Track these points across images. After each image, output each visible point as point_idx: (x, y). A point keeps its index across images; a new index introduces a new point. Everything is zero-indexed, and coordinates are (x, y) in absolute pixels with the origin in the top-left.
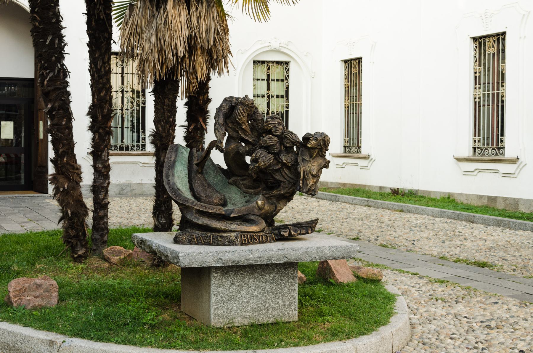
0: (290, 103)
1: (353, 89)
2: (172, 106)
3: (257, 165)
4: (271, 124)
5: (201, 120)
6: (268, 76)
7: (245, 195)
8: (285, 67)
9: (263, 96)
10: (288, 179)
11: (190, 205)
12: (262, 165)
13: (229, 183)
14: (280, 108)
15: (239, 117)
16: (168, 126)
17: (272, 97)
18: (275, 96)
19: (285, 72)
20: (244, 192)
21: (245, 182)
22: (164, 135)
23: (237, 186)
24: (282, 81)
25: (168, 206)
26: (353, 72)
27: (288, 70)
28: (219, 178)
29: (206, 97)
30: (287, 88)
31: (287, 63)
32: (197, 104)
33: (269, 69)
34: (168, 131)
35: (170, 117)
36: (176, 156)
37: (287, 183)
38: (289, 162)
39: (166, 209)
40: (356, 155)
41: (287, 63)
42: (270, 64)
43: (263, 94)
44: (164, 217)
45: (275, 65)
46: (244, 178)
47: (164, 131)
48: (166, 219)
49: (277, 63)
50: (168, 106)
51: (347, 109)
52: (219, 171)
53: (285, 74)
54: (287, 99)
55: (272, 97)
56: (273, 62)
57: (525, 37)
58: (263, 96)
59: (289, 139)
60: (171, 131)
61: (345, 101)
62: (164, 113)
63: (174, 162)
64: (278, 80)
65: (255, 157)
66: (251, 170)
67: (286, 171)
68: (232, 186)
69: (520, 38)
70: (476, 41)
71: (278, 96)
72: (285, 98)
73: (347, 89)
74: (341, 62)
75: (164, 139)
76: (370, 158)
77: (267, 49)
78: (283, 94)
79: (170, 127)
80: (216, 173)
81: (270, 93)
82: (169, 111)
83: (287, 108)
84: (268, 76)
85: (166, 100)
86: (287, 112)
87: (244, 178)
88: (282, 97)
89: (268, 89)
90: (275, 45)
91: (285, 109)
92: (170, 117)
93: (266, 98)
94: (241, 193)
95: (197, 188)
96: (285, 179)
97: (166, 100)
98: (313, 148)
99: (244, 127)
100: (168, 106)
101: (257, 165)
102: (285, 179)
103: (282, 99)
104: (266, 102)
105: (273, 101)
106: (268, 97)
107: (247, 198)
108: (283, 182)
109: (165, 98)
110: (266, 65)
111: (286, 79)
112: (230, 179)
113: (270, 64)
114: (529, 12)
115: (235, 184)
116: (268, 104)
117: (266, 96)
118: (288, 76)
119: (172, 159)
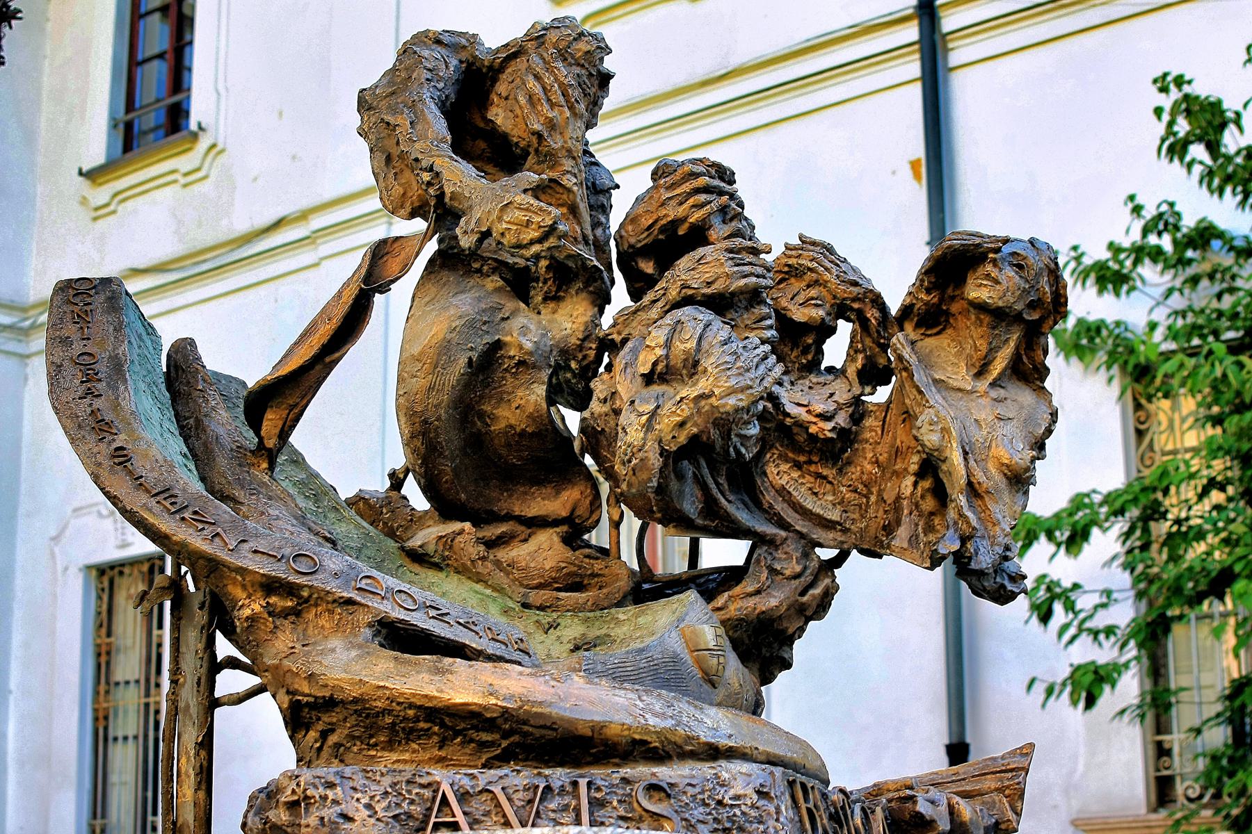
12: (732, 391)
73: (103, 659)
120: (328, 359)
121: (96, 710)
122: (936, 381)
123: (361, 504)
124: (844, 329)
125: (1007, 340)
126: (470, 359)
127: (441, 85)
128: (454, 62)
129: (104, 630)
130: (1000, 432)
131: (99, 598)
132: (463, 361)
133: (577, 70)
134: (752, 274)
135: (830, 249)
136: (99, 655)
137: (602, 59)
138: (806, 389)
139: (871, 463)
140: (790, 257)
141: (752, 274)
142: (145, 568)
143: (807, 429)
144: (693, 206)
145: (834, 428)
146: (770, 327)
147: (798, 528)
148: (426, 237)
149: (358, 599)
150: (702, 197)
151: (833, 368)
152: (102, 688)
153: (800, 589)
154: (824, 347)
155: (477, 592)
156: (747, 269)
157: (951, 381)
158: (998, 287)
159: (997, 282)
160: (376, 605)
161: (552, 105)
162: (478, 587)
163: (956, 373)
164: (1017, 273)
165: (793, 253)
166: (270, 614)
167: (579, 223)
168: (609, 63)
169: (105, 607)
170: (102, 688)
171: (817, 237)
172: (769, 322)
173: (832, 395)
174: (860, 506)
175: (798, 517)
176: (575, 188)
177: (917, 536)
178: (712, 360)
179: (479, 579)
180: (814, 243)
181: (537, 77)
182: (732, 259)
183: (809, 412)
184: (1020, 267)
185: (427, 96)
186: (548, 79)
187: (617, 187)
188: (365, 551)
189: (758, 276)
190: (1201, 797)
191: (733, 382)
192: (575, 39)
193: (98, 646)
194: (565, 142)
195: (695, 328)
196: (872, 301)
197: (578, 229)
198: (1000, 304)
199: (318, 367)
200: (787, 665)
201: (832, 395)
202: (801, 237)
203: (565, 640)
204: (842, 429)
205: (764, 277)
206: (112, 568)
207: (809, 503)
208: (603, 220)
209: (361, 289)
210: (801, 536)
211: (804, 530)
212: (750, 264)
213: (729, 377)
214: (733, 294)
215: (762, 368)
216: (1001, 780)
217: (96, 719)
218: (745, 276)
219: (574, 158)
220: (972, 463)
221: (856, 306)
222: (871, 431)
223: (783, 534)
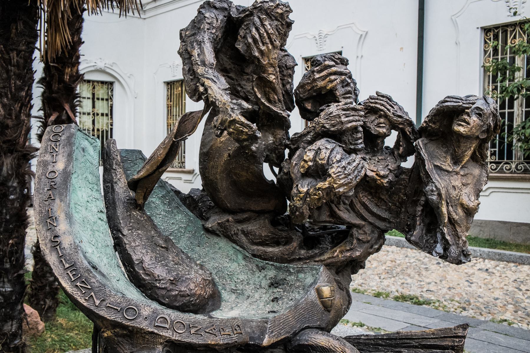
0: (114, 121)
1: (176, 109)
2: (24, 68)
3: (324, 185)
4: (335, 73)
5: (67, 107)
6: (93, 95)
7: (262, 263)
8: (109, 87)
9: (89, 114)
10: (371, 219)
11: (144, 325)
13: (207, 231)
14: (105, 125)
15: (263, 48)
16: (17, 106)
17: (98, 114)
18: (100, 114)
19: (110, 91)
20: (254, 256)
21: (249, 227)
22: (10, 122)
23: (231, 238)
24: (107, 100)
25: (17, 260)
26: (175, 93)
27: (112, 90)
28: (179, 217)
29: (75, 70)
30: (112, 107)
31: (112, 83)
32: (61, 80)
33: (94, 88)
34: (18, 117)
35: (21, 89)
36: (70, 157)
37: (368, 229)
38: (383, 177)
39: (13, 266)
40: (180, 169)
41: (112, 83)
42: (95, 84)
43: (89, 112)
44: (9, 281)
45: (100, 84)
46: (245, 216)
47: (10, 115)
48: (13, 285)
49: (103, 83)
50: (18, 66)
51: (169, 127)
52: (177, 200)
53: (110, 93)
54: (112, 118)
55: (98, 114)
56: (98, 82)
57: (362, 56)
58: (89, 114)
59: (386, 116)
60: (23, 117)
61: (168, 120)
62: (9, 78)
63: (67, 175)
64: (102, 99)
65: (314, 160)
66: (304, 199)
67: (365, 200)
68: (216, 240)
69: (357, 57)
70: (308, 60)
71: (102, 115)
72: (110, 116)
73: (169, 108)
74: (163, 84)
75: (8, 132)
76: (195, 173)
77: (92, 69)
78: (107, 112)
79: (21, 108)
80: (169, 204)
81: (96, 112)
82: (19, 77)
83: (112, 125)
84: (93, 95)
85: (14, 55)
86: (111, 129)
87: (245, 216)
88: (107, 115)
89: (94, 107)
90: (101, 65)
91: (110, 127)
92: (23, 90)
93: (91, 115)
94: (245, 258)
95: (141, 254)
96: (364, 219)
97: (14, 55)
98: (467, 138)
99: (272, 78)
100: (18, 66)
101: (324, 185)
102: (364, 219)
103: (107, 117)
104: (91, 119)
105: (99, 119)
106: (94, 114)
107: (271, 273)
108: (359, 227)
109: (12, 50)
110: (91, 84)
111: (111, 98)
112: (207, 219)
113: (95, 84)
114: (367, 33)
115: (224, 233)
116: (93, 122)
117: (91, 114)
118: (112, 95)
119: (60, 166)
120: (160, 170)
121: (168, 123)
122: (436, 167)
123: (190, 199)
124: (394, 134)
125: (470, 147)
126: (229, 154)
127: (214, 31)
128: (221, 17)
129: (169, 100)
130: (464, 191)
131: (168, 91)
132: (226, 155)
133: (276, 23)
134: (353, 121)
135: (390, 99)
136: (168, 107)
137: (287, 17)
138: (376, 162)
139: (403, 195)
140: (372, 103)
141: (353, 121)
142: (180, 83)
143: (376, 182)
144: (329, 82)
145: (388, 182)
146: (361, 143)
147: (370, 220)
148: (204, 112)
149: (156, 331)
150: (333, 77)
151: (388, 147)
152: (169, 117)
153: (370, 246)
154: (385, 140)
155: (234, 248)
156: (351, 118)
157: (442, 166)
158: (469, 126)
159: (468, 123)
160: (164, 334)
161: (263, 44)
162: (234, 245)
163: (445, 162)
164: (478, 118)
165: (373, 101)
166: (115, 336)
167: (276, 95)
168: (291, 16)
169: (169, 94)
170: (169, 117)
171: (384, 92)
172: (360, 141)
173: (387, 165)
174: (397, 211)
175: (370, 215)
176: (274, 81)
177: (423, 236)
178: (333, 170)
179: (234, 242)
180: (383, 96)
181: (257, 29)
182: (345, 114)
183: (377, 174)
184: (480, 115)
185: (206, 37)
186: (262, 31)
187: (297, 65)
188: (188, 228)
189: (356, 121)
190: (496, 169)
191: (342, 181)
192: (275, 8)
193: (168, 105)
194: (269, 60)
195: (326, 153)
196: (408, 124)
197: (276, 97)
198: (469, 133)
199: (157, 173)
200: (363, 267)
201: (387, 165)
202: (377, 93)
203: (268, 277)
204: (391, 181)
205: (359, 121)
206: (171, 82)
207: (375, 210)
208: (290, 81)
209: (174, 141)
210: (371, 223)
211: (372, 221)
212: (353, 116)
213: (340, 179)
214: (344, 131)
215: (356, 172)
216: (454, 342)
217: (168, 126)
218: (351, 122)
219: (274, 67)
220: (450, 208)
221: (401, 126)
222: (404, 180)
223: (363, 223)
